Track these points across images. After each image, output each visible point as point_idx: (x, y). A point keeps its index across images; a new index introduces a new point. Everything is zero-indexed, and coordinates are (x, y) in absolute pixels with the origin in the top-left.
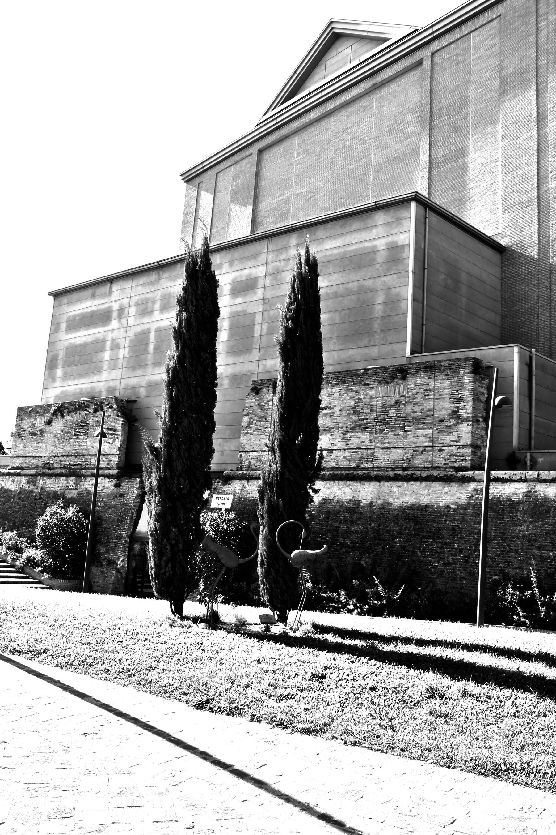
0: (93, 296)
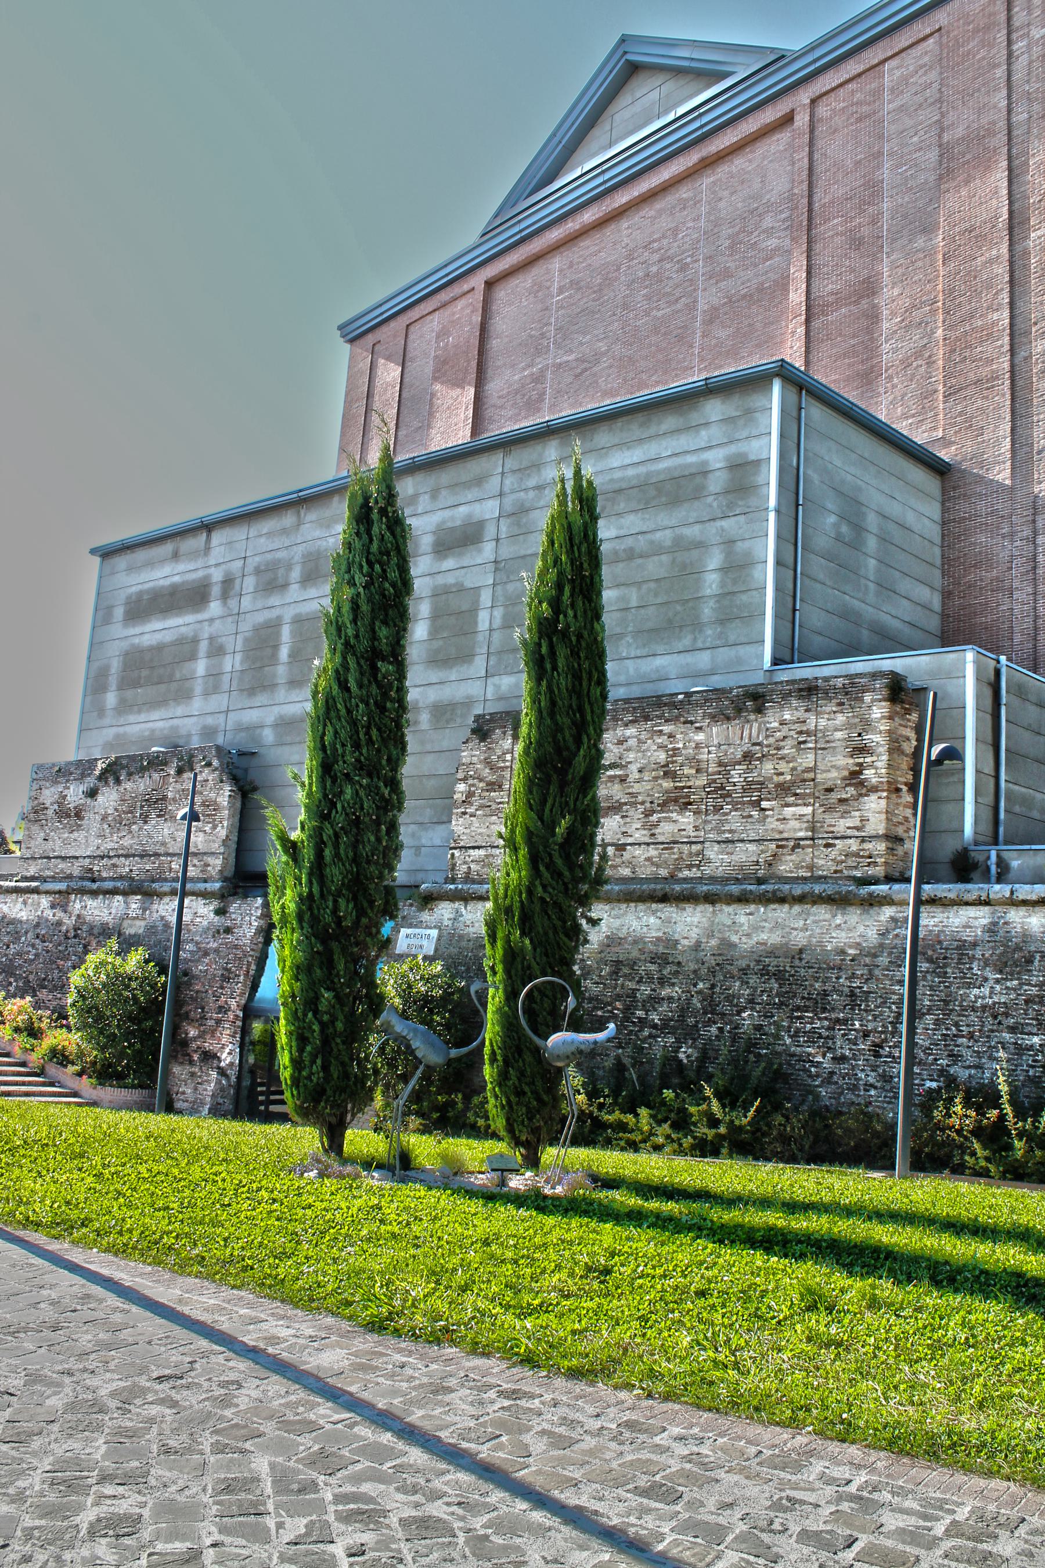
0: (176, 556)
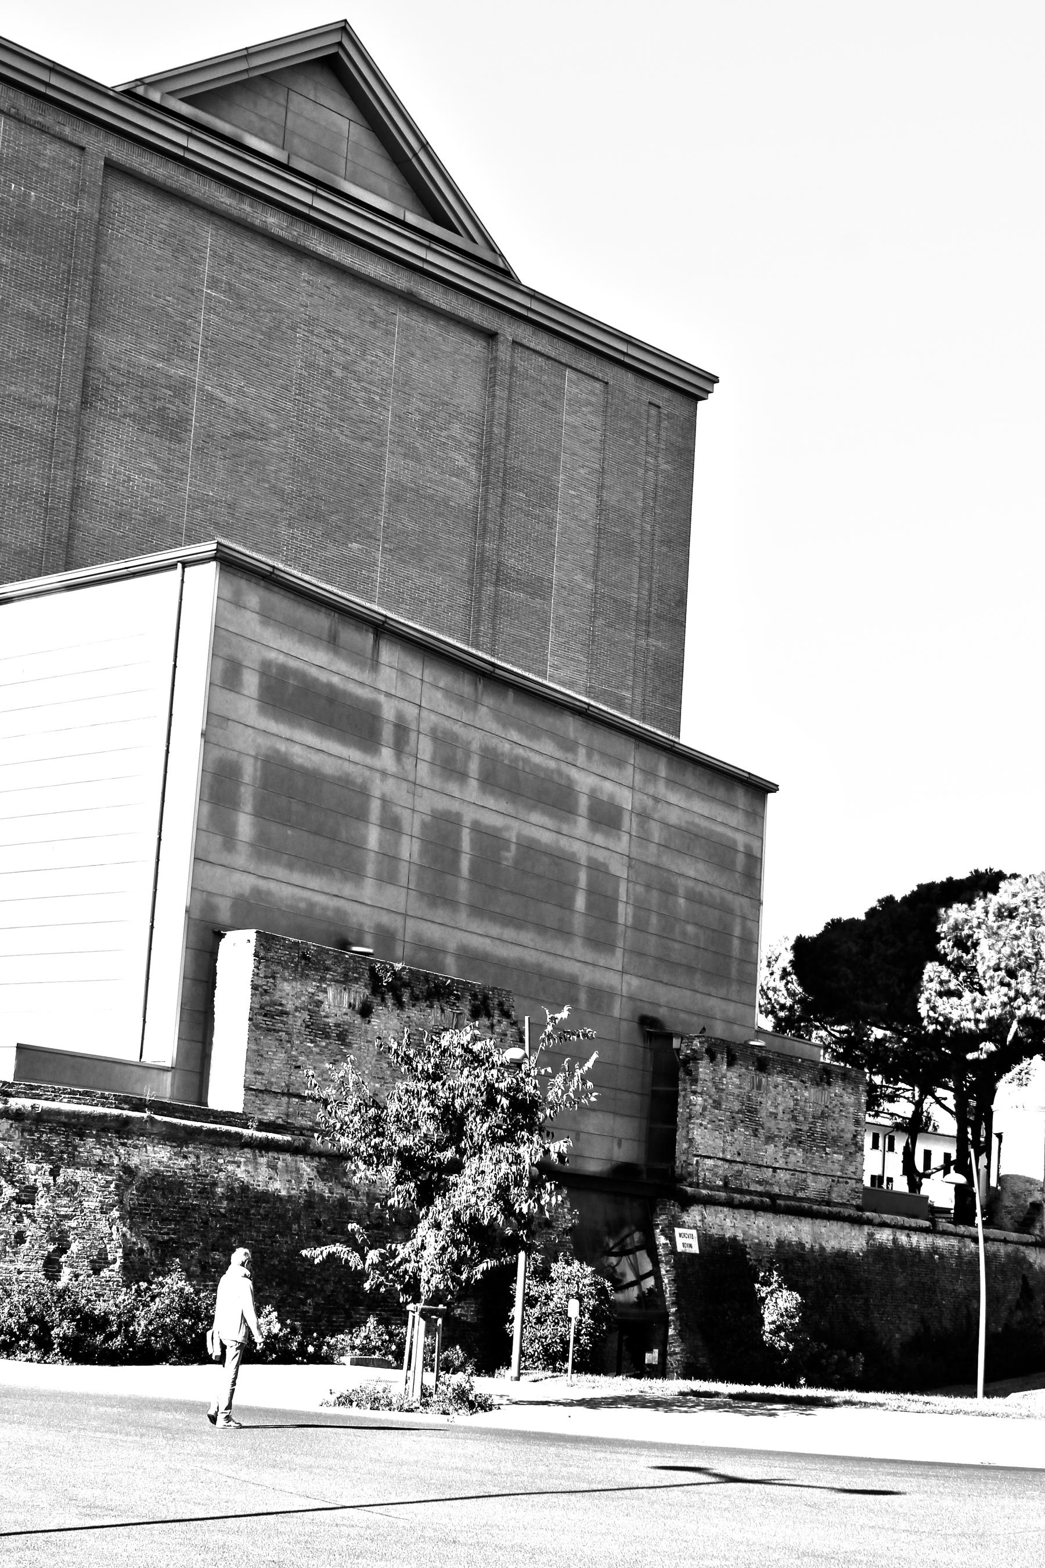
0: (333, 643)
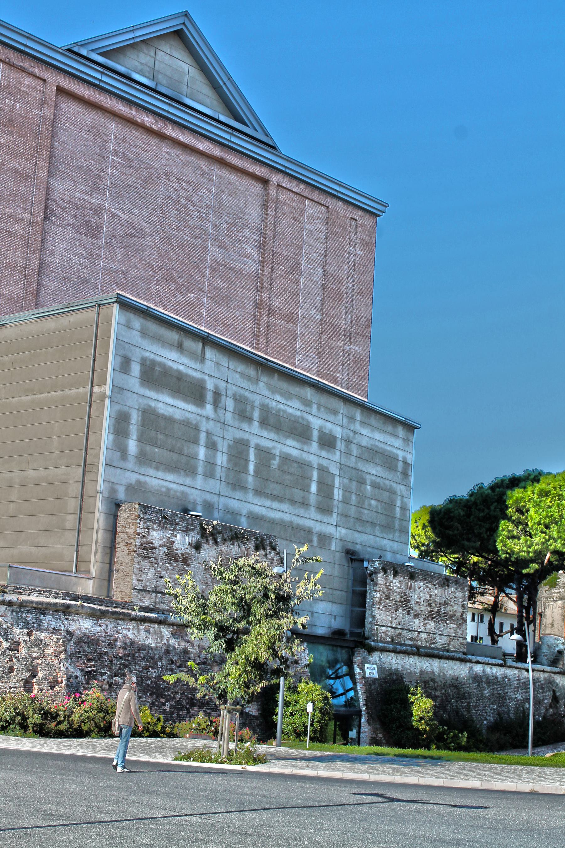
0: (180, 347)
